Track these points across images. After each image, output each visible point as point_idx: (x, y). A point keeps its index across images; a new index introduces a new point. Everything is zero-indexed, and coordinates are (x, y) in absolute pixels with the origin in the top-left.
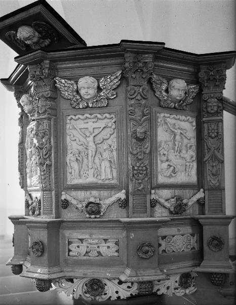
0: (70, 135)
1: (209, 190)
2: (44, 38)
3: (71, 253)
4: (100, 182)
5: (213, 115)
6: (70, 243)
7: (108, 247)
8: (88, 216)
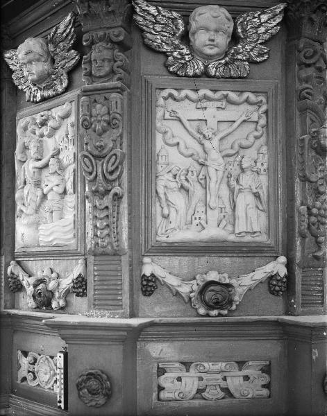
3: (164, 395)
4: (232, 238)
6: (161, 371)
7: (246, 378)
8: (202, 311)
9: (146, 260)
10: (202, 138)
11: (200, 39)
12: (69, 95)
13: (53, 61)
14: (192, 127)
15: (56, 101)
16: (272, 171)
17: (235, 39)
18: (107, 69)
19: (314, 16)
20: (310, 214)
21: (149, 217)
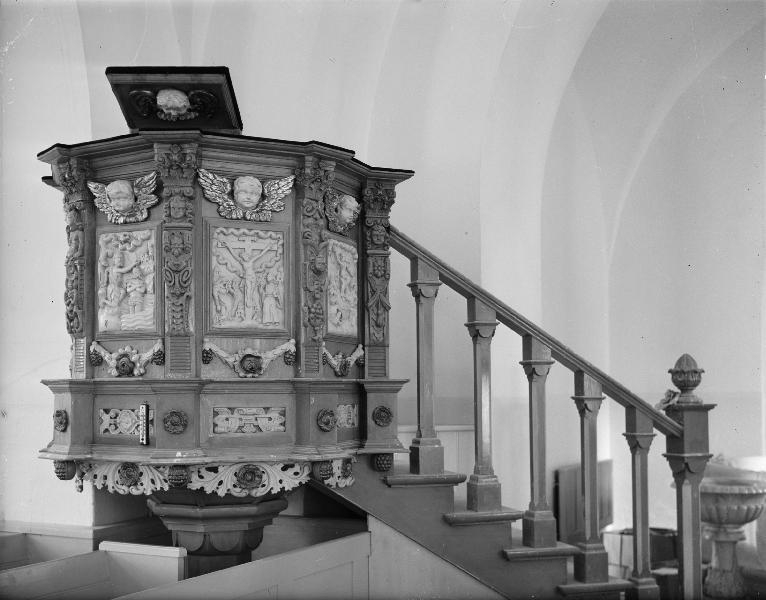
0: (218, 256)
1: (370, 346)
2: (194, 110)
3: (217, 429)
4: (261, 326)
5: (378, 246)
6: (216, 414)
7: (270, 419)
8: (242, 374)
9: (206, 340)
10: (242, 261)
11: (241, 197)
12: (148, 224)
13: (136, 199)
14: (236, 253)
15: (137, 227)
16: (286, 283)
17: (263, 197)
18: (182, 214)
19: (312, 186)
20: (310, 312)
21: (208, 312)
